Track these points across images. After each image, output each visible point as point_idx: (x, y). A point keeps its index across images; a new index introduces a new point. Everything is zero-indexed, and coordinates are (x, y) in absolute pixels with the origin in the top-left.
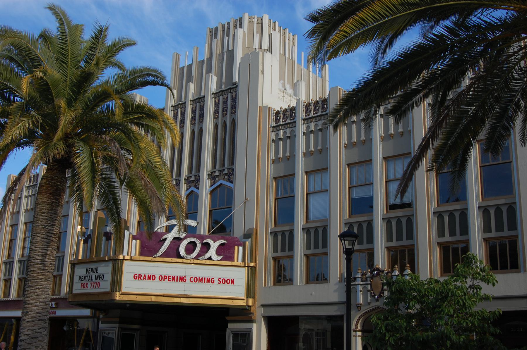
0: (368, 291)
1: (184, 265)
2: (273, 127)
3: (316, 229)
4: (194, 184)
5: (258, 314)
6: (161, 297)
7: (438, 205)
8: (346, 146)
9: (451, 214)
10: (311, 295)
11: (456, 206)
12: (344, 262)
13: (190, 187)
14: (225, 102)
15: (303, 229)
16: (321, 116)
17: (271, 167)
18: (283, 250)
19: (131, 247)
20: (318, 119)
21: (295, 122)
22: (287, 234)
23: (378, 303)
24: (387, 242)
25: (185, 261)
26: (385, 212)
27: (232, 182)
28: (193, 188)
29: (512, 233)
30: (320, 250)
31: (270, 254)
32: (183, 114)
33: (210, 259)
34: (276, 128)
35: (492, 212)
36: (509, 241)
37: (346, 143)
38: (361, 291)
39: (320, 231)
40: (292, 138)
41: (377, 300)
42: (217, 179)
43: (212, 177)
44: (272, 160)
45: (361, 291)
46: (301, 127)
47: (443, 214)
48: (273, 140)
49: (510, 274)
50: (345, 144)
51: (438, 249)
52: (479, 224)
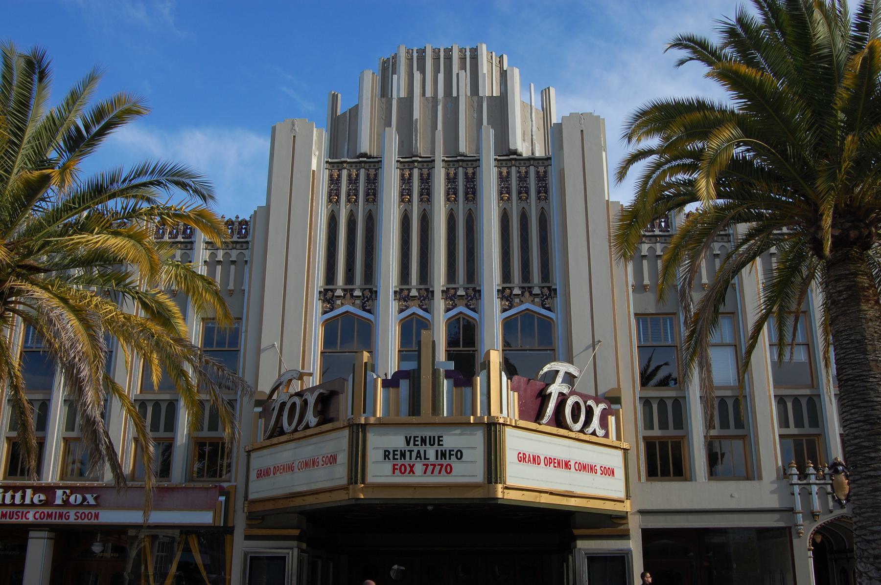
0: (829, 493)
1: (567, 441)
4: (465, 302)
5: (635, 525)
10: (731, 496)
11: (668, 393)
13: (407, 307)
14: (353, 181)
16: (237, 242)
19: (502, 397)
21: (192, 243)
23: (844, 511)
27: (369, 311)
28: (415, 309)
29: (679, 433)
33: (594, 433)
41: (842, 506)
42: (339, 302)
43: (505, 295)
47: (147, 403)
48: (205, 262)
51: (6, 445)
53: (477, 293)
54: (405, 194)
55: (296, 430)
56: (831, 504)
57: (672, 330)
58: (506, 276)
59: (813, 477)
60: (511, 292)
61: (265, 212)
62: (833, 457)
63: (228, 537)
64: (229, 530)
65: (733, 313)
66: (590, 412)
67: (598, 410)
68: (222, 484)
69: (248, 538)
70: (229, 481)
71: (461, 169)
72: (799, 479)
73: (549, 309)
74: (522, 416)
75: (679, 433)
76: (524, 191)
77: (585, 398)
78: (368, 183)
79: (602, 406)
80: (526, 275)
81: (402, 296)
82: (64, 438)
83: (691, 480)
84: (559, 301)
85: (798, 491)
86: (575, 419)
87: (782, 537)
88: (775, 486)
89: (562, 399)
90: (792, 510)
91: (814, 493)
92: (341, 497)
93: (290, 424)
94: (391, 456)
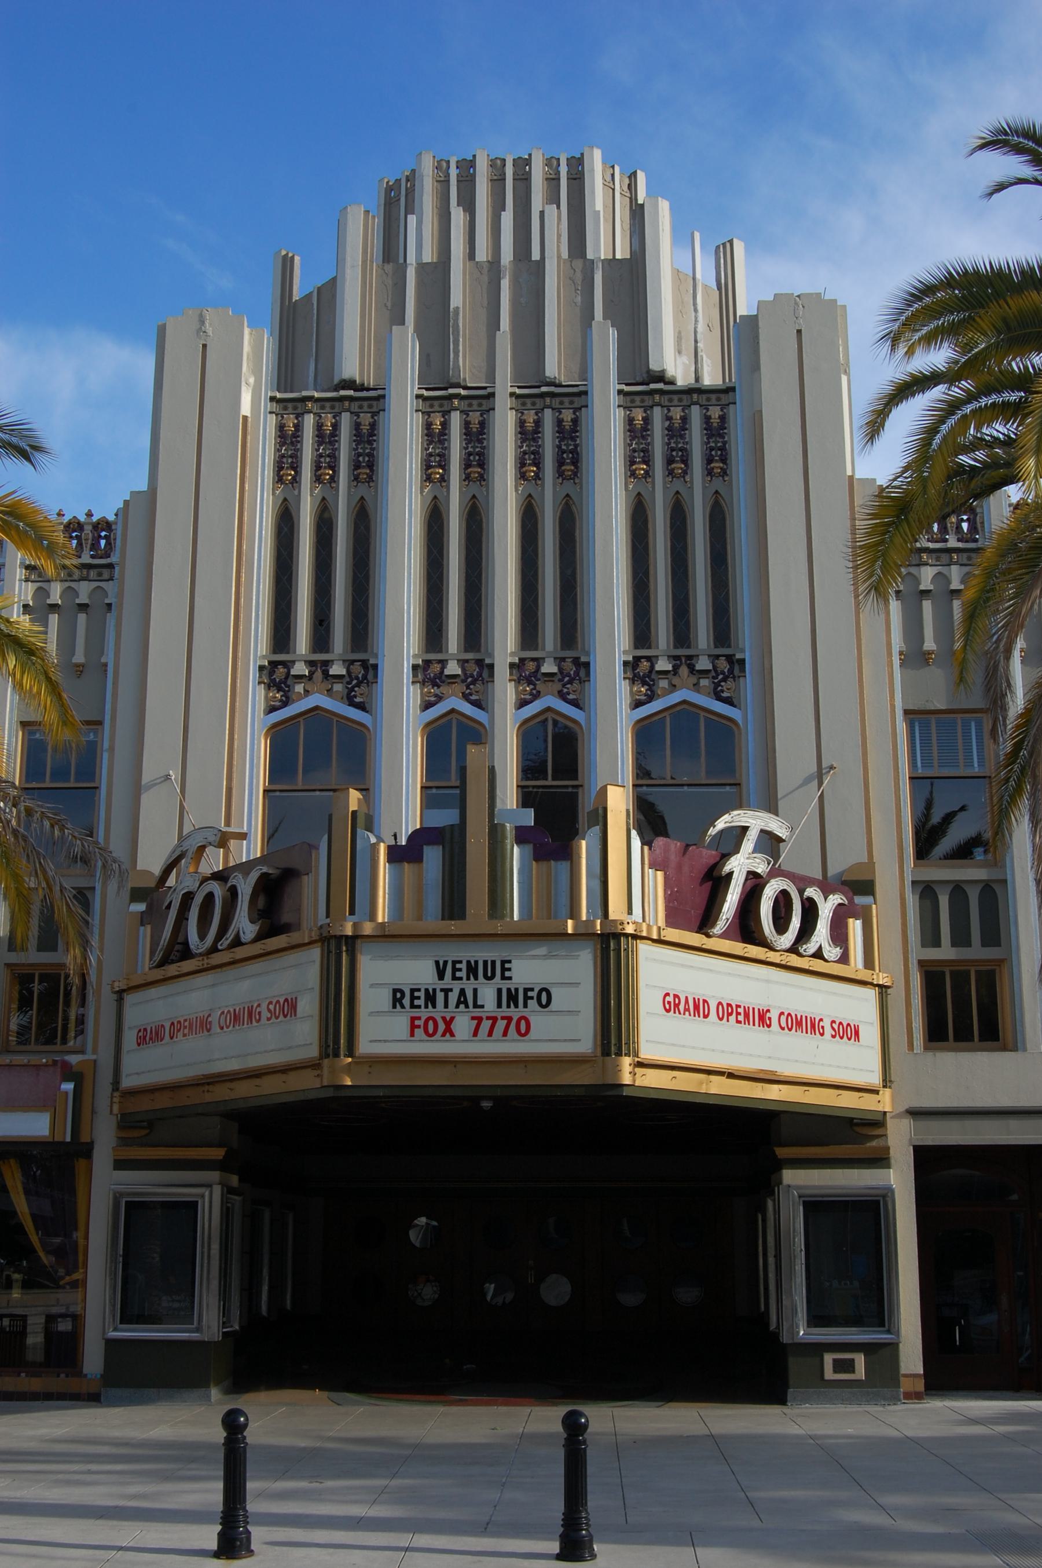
4: (558, 686)
6: (723, 1079)
8: (906, 660)
12: (114, 1005)
13: (440, 698)
14: (326, 438)
19: (631, 880)
20: (106, 576)
24: (923, 946)
25: (772, 957)
29: (991, 953)
32: (478, 437)
33: (818, 955)
36: (976, 971)
43: (640, 672)
48: (26, 606)
53: (583, 668)
54: (434, 465)
55: (214, 949)
58: (642, 634)
60: (652, 667)
61: (145, 505)
63: (81, 1163)
64: (86, 1151)
66: (810, 911)
67: (826, 908)
68: (67, 1058)
69: (120, 1165)
70: (82, 1052)
71: (548, 412)
73: (729, 701)
74: (673, 919)
75: (991, 953)
76: (677, 458)
77: (802, 882)
78: (358, 443)
79: (835, 899)
80: (682, 633)
81: (429, 675)
84: (749, 685)
86: (781, 924)
89: (755, 884)
92: (305, 1084)
93: (202, 936)
94: (406, 1001)
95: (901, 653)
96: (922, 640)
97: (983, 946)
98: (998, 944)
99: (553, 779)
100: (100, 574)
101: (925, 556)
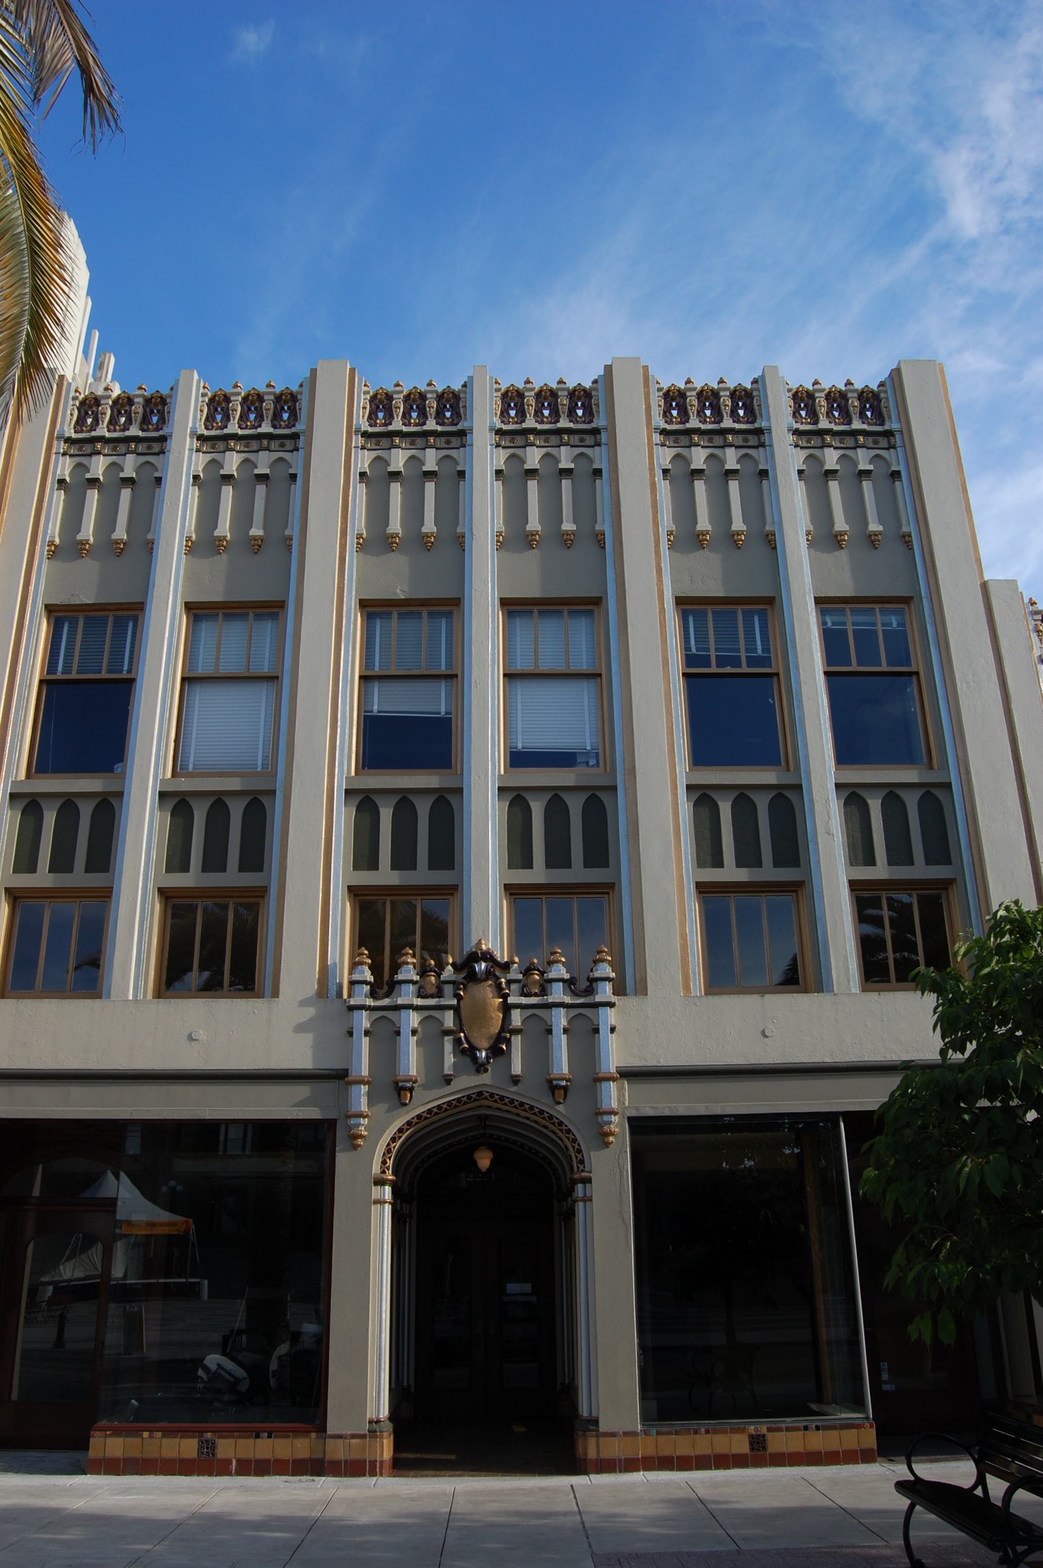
0: (447, 1032)
2: (69, 440)
3: (219, 803)
7: (28, 776)
8: (55, 553)
9: (68, 805)
10: (191, 1038)
15: (163, 795)
17: (43, 567)
18: (61, 863)
21: (163, 439)
22: (86, 811)
23: (486, 1079)
26: (169, 775)
29: (249, 880)
30: (79, 878)
31: (342, 872)
34: (380, 439)
35: (537, 808)
37: (57, 541)
38: (414, 1032)
39: (236, 810)
40: (149, 486)
41: (480, 1068)
44: (51, 543)
45: (414, 1032)
46: (186, 460)
47: (378, 800)
48: (196, 477)
49: (725, 998)
50: (51, 543)
52: (155, 840)
56: (449, 1059)
57: (30, 632)
59: (608, 987)
62: (474, 941)
65: (906, 600)
72: (373, 995)
75: (249, 880)
82: (161, 891)
83: (820, 989)
85: (564, 1022)
87: (312, 1143)
88: (310, 1012)
90: (341, 1076)
91: (406, 1032)
95: (670, 533)
96: (729, 521)
97: (430, 868)
98: (605, 864)
99: (718, 666)
100: (582, 440)
101: (828, 438)
